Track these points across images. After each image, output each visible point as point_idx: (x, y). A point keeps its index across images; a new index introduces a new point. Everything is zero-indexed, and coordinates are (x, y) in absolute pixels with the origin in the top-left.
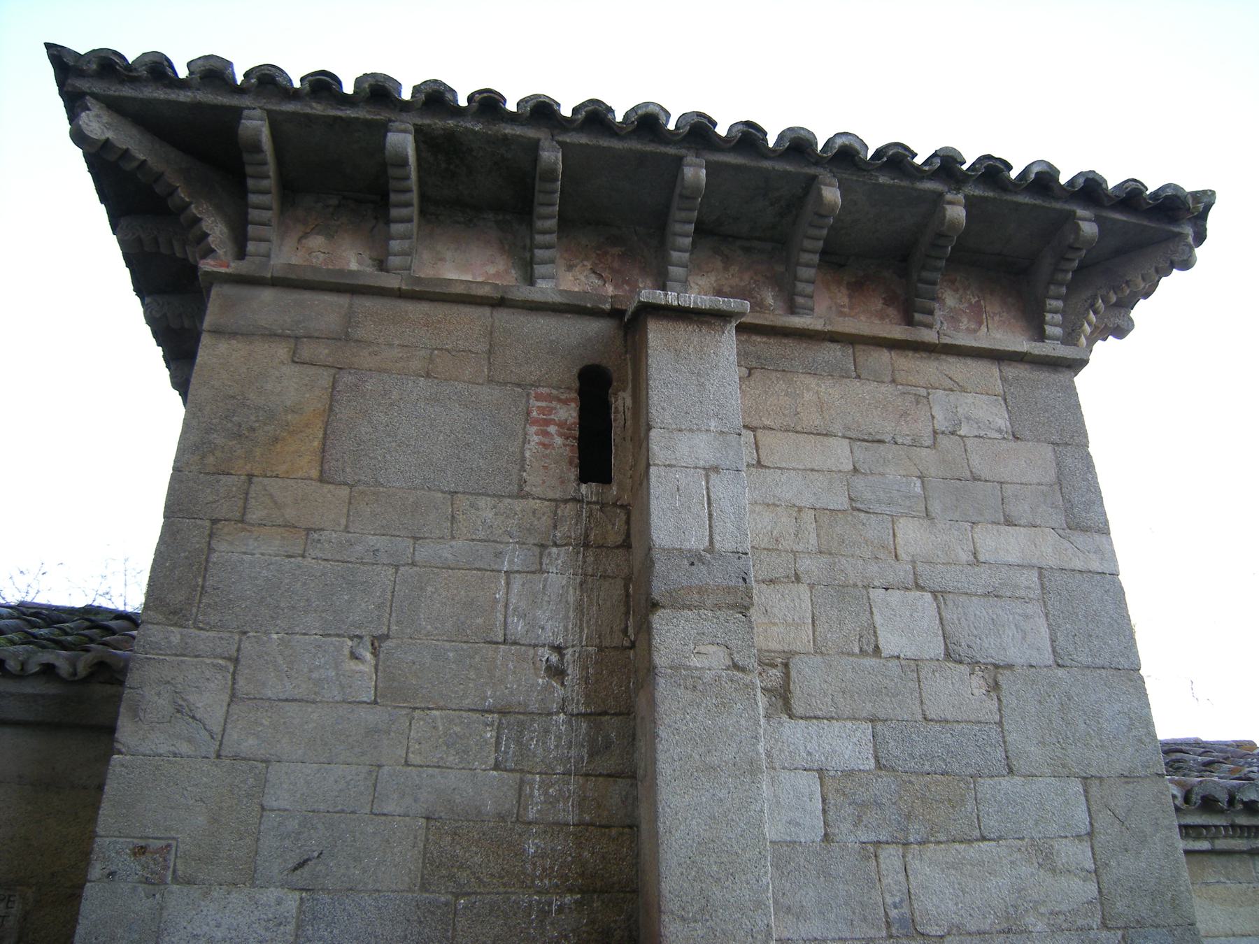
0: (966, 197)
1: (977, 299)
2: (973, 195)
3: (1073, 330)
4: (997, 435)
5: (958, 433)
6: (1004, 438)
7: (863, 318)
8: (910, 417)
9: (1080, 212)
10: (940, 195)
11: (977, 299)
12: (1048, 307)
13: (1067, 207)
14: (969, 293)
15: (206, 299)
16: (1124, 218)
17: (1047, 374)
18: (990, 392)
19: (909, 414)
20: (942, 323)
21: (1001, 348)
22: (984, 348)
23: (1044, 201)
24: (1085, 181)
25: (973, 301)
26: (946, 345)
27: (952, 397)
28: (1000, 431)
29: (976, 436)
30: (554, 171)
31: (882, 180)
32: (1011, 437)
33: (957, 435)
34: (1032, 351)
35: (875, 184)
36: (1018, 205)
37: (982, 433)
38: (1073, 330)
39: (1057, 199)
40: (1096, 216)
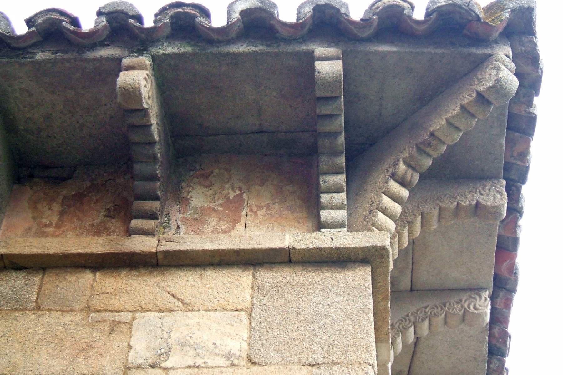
0: (154, 58)
1: (238, 192)
2: (164, 54)
3: (370, 212)
4: (222, 362)
5: (163, 365)
6: (233, 365)
7: (70, 235)
8: (94, 351)
9: (320, 50)
10: (119, 60)
11: (238, 192)
12: (322, 185)
13: (304, 47)
14: (227, 186)
15: (503, 348)
16: (394, 49)
17: (327, 274)
18: (229, 307)
19: (94, 348)
20: (178, 227)
21: (248, 247)
22: (223, 250)
23: (268, 46)
24: (314, 9)
25: (232, 195)
26: (167, 253)
27: (168, 319)
28: (228, 356)
29: (189, 367)
30: (342, 187)
31: (39, 56)
32: (244, 363)
33: (161, 368)
34: (297, 246)
35: (32, 62)
36: (236, 55)
37: (199, 362)
38: (370, 212)
39: (288, 41)
40: (344, 53)
